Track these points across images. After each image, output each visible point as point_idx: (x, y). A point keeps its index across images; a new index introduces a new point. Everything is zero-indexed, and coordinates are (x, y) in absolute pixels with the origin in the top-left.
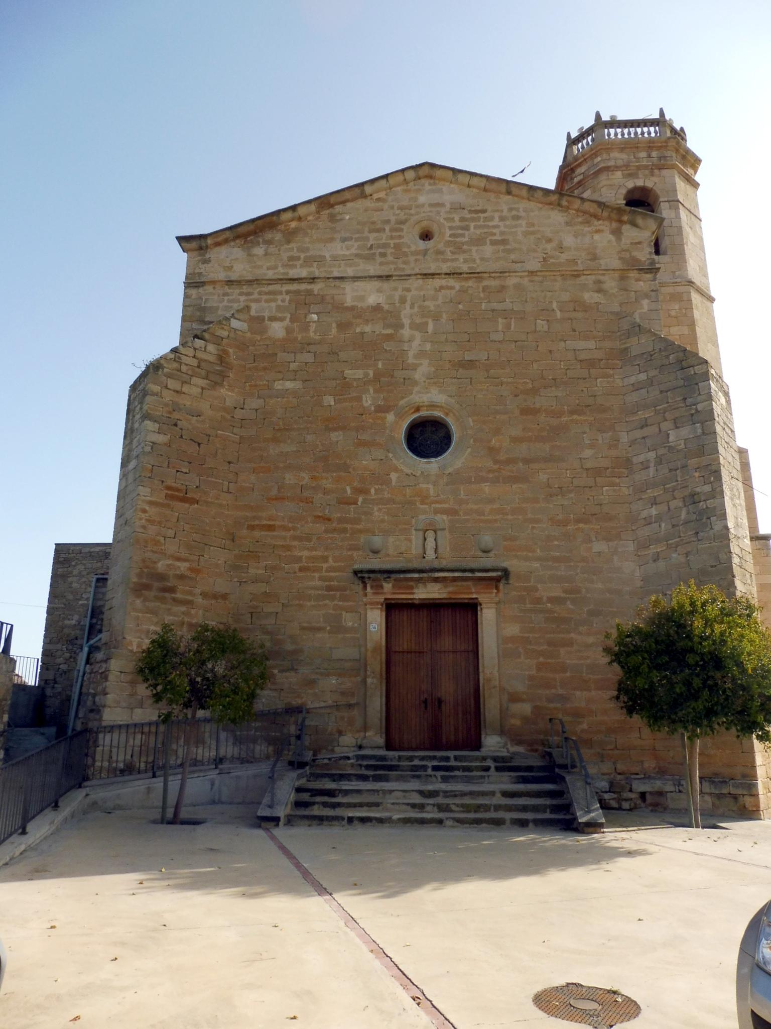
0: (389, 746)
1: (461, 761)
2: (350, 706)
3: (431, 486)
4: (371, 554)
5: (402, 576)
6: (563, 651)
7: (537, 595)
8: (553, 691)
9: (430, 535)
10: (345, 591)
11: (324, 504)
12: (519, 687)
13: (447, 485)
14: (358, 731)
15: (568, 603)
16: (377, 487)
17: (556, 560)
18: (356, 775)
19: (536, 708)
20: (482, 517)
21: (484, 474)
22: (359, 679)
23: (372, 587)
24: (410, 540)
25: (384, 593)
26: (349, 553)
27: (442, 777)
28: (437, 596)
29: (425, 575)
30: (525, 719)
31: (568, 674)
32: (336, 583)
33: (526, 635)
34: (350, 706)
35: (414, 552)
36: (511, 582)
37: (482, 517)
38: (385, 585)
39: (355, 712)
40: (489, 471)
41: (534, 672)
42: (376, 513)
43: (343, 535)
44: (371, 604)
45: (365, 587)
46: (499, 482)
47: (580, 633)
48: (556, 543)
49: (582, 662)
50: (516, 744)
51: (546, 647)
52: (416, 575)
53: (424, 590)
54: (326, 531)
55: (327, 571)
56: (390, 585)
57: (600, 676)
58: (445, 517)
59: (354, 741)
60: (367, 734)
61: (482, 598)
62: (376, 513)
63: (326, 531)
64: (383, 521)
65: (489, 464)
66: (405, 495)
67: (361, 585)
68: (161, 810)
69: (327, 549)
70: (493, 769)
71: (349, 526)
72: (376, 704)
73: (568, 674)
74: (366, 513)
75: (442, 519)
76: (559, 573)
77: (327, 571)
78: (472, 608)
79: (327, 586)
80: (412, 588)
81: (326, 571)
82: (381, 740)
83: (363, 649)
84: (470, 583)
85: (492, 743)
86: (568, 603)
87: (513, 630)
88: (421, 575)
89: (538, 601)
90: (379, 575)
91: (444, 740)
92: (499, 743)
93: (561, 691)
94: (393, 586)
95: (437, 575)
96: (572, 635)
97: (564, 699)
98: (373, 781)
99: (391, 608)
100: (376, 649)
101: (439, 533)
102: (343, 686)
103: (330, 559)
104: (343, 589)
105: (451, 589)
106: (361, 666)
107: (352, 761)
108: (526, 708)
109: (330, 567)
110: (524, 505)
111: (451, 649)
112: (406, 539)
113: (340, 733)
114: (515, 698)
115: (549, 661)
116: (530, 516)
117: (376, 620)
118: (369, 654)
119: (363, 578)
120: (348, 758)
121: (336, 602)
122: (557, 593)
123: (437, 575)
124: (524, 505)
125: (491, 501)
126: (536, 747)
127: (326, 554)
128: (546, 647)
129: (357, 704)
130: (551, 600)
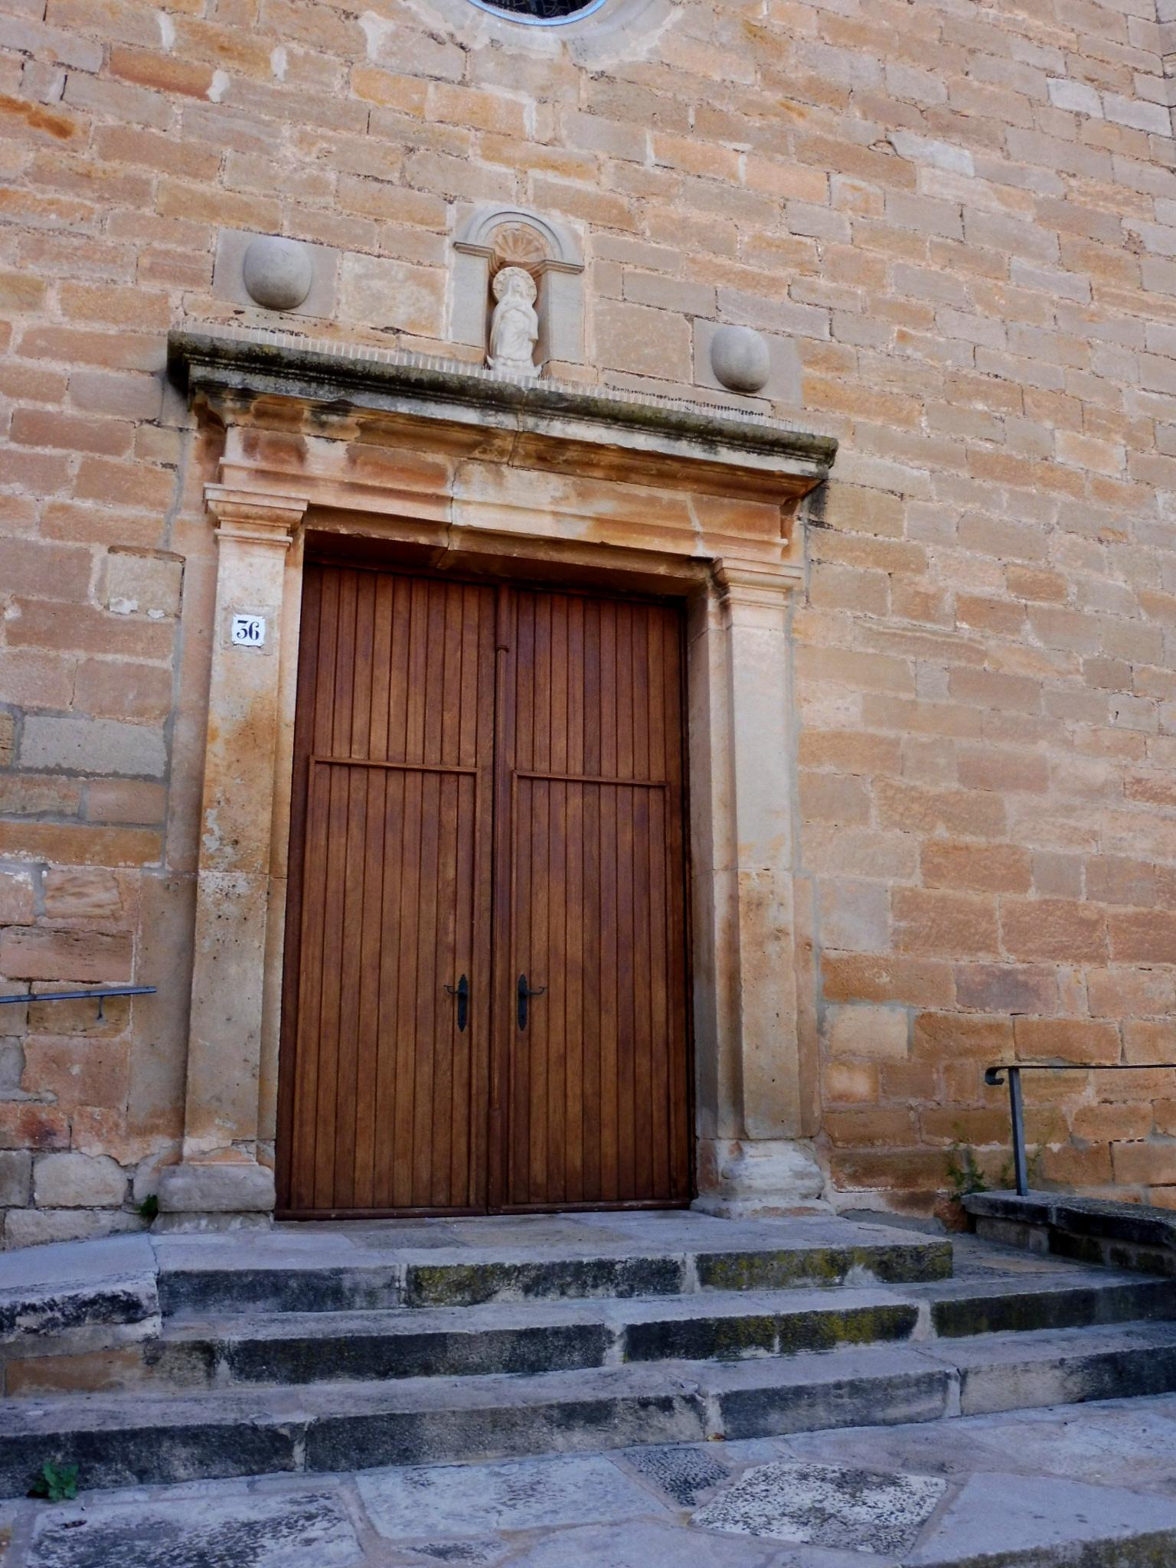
0: (292, 1206)
1: (732, 1283)
2: (102, 1003)
3: (528, 101)
4: (252, 310)
5: (404, 407)
6: (1013, 803)
7: (923, 583)
8: (985, 959)
9: (516, 288)
10: (116, 449)
11: (42, 56)
12: (865, 938)
13: (591, 110)
14: (143, 1131)
15: (1028, 626)
16: (299, 50)
17: (982, 465)
18: (190, 1435)
19: (926, 1023)
20: (722, 260)
21: (729, 108)
22: (157, 870)
23: (250, 446)
24: (433, 286)
25: (309, 481)
26: (151, 287)
27: (731, 1403)
28: (545, 527)
29: (508, 421)
30: (885, 1072)
31: (1032, 895)
32: (69, 410)
33: (889, 733)
34: (102, 1003)
35: (447, 336)
36: (831, 518)
37: (722, 260)
38: (315, 446)
39: (129, 1036)
40: (749, 107)
41: (915, 881)
42: (289, 151)
43: (123, 208)
44: (242, 519)
45: (214, 446)
46: (781, 149)
47: (1068, 744)
48: (980, 406)
49: (1076, 850)
50: (856, 1178)
51: (955, 786)
52: (470, 416)
53: (492, 495)
54: (40, 175)
55: (28, 349)
56: (339, 450)
57: (1131, 909)
58: (580, 226)
59: (117, 1180)
60: (191, 1145)
61: (735, 561)
62: (289, 151)
63: (40, 175)
64: (316, 186)
65: (749, 79)
66: (419, 110)
67: (195, 437)
68: (620, 788)
69: (37, 250)
70: (924, 1326)
71: (156, 176)
72: (242, 993)
73: (1032, 895)
74: (242, 142)
75: (573, 235)
76: (995, 515)
77: (28, 349)
78: (665, 609)
79: (18, 416)
80: (438, 475)
81: (22, 351)
82: (259, 1179)
83: (185, 731)
84: (683, 496)
85: (770, 1176)
86: (1028, 626)
87: (838, 707)
88: (492, 420)
89: (925, 606)
90: (294, 388)
91: (538, 1167)
92: (801, 1175)
93: (1008, 961)
94: (353, 460)
95: (559, 428)
96: (1043, 747)
97: (1015, 989)
98: (316, 1464)
99: (340, 560)
100: (251, 733)
101: (555, 280)
102: (70, 904)
103: (52, 299)
104: (107, 442)
105: (605, 506)
106: (184, 801)
107: (151, 1326)
108: (886, 1027)
109: (43, 333)
110: (873, 253)
111: (576, 770)
112: (413, 276)
113: (42, 1137)
114: (845, 984)
115: (968, 839)
116: (891, 292)
117: (261, 593)
118: (218, 752)
119: (214, 389)
120: (129, 1308)
121: (62, 497)
122: (990, 587)
123: (559, 428)
124: (873, 253)
125: (756, 208)
126: (924, 1186)
127: (33, 270)
128: (955, 786)
129: (144, 993)
130: (976, 609)
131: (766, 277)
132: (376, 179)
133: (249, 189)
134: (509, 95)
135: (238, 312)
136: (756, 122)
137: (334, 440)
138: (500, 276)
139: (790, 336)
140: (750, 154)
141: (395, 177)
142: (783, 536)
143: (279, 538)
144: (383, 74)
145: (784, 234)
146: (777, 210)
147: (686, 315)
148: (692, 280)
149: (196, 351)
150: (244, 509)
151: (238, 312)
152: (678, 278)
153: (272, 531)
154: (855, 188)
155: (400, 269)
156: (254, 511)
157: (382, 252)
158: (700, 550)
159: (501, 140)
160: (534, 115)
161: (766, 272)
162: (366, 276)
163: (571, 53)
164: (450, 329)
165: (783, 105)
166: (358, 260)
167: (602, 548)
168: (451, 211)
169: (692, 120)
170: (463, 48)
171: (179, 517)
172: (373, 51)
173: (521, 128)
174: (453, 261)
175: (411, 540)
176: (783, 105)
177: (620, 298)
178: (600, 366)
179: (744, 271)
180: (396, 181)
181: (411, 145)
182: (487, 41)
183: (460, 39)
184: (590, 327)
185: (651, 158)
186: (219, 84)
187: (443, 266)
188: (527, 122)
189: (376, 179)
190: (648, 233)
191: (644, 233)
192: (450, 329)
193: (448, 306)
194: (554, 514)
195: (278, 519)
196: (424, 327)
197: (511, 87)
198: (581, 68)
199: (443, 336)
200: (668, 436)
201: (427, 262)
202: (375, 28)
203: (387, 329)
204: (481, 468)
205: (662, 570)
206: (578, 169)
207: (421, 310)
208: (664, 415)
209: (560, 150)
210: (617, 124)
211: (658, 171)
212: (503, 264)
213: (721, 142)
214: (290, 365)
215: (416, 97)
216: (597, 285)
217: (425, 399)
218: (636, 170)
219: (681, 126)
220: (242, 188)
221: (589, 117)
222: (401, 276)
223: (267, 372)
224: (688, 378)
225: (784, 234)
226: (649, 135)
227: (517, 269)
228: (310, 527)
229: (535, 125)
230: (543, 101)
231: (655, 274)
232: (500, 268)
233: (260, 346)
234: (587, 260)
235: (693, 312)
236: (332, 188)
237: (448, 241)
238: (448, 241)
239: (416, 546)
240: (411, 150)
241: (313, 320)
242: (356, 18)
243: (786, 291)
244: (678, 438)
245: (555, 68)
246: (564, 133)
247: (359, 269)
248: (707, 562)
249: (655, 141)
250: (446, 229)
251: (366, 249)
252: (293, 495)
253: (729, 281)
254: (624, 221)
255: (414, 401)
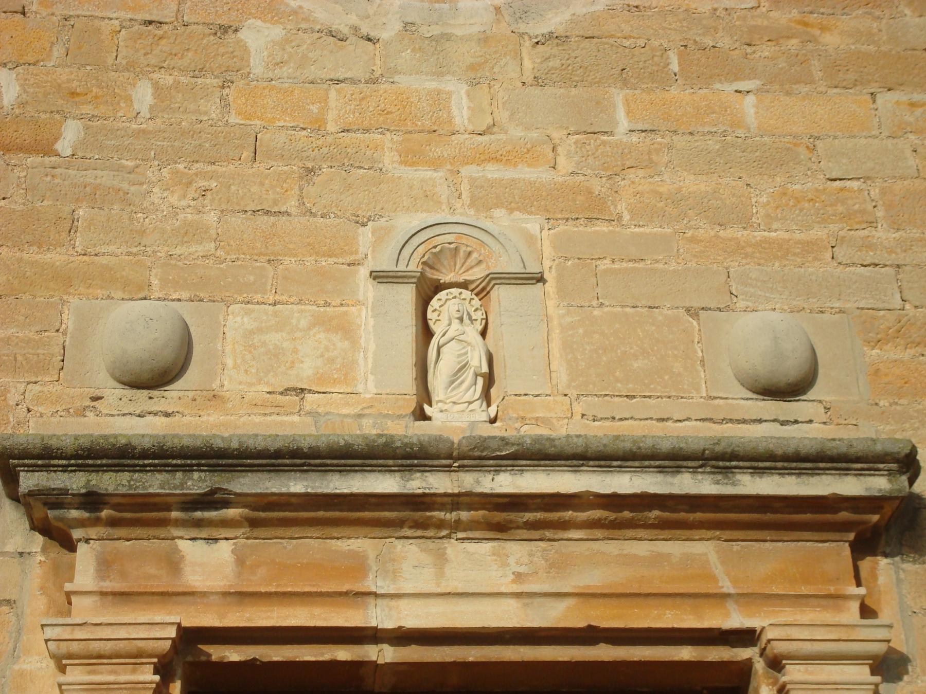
13: (537, 81)
24: (346, 329)
58: (533, 224)
64: (191, 233)
66: (318, 126)
112: (319, 322)
131: (799, 242)
132: (268, 212)
133: (111, 249)
134: (431, 85)
135: (96, 399)
136: (766, 51)
137: (216, 540)
138: (434, 303)
139: (841, 311)
140: (758, 91)
141: (291, 205)
142: (859, 584)
143: (141, 678)
144: (273, 87)
145: (818, 183)
146: (803, 153)
147: (688, 310)
148: (693, 265)
149: (25, 454)
150: (96, 646)
151: (96, 399)
152: (673, 266)
153: (134, 672)
154: (913, 105)
155: (300, 315)
156: (108, 647)
157: (278, 298)
158: (735, 620)
159: (424, 136)
160: (465, 101)
161: (798, 236)
162: (260, 330)
163: (507, 18)
164: (371, 378)
165: (799, 22)
166: (248, 313)
167: (590, 635)
168: (365, 236)
169: (675, 67)
170: (369, 40)
171: (16, 667)
172: (257, 67)
173: (450, 120)
174: (370, 295)
175: (326, 657)
176: (799, 22)
177: (595, 303)
178: (573, 393)
179: (765, 240)
180: (293, 211)
181: (310, 165)
182: (398, 26)
183: (365, 30)
184: (556, 346)
185: (623, 124)
186: (70, 136)
187: (358, 303)
188: (455, 111)
189: (268, 212)
190: (626, 217)
191: (620, 218)
192: (371, 378)
193: (366, 351)
194: (518, 595)
195: (139, 654)
196: (335, 382)
197: (434, 74)
198: (522, 35)
199: (360, 388)
200: (661, 469)
201: (338, 302)
202: (258, 38)
203: (286, 391)
204: (413, 547)
205: (686, 653)
206: (525, 154)
207: (332, 361)
208: (123, 441)
209: (502, 136)
210: (574, 91)
211: (635, 138)
212: (438, 287)
213: (718, 86)
214: (145, 454)
215: (315, 108)
216: (562, 292)
217: (324, 470)
218: (604, 143)
219: (660, 78)
220: (98, 249)
221: (537, 91)
222: (303, 323)
223: (118, 468)
224: (698, 390)
225: (818, 183)
226: (619, 96)
227: (455, 291)
228: (190, 659)
229: (466, 113)
230: (474, 84)
231: (641, 265)
232: (436, 293)
233: (105, 437)
234: (547, 263)
235: (696, 304)
236: (213, 232)
237: (363, 272)
238: (363, 272)
239: (334, 664)
240: (311, 171)
241: (191, 394)
242: (236, 31)
243: (828, 255)
244: (677, 470)
245: (484, 39)
246: (502, 116)
247: (248, 323)
248: (747, 637)
249: (627, 102)
250: (360, 256)
251: (258, 297)
252: (158, 619)
253: (747, 256)
254: (594, 209)
255: (313, 475)
